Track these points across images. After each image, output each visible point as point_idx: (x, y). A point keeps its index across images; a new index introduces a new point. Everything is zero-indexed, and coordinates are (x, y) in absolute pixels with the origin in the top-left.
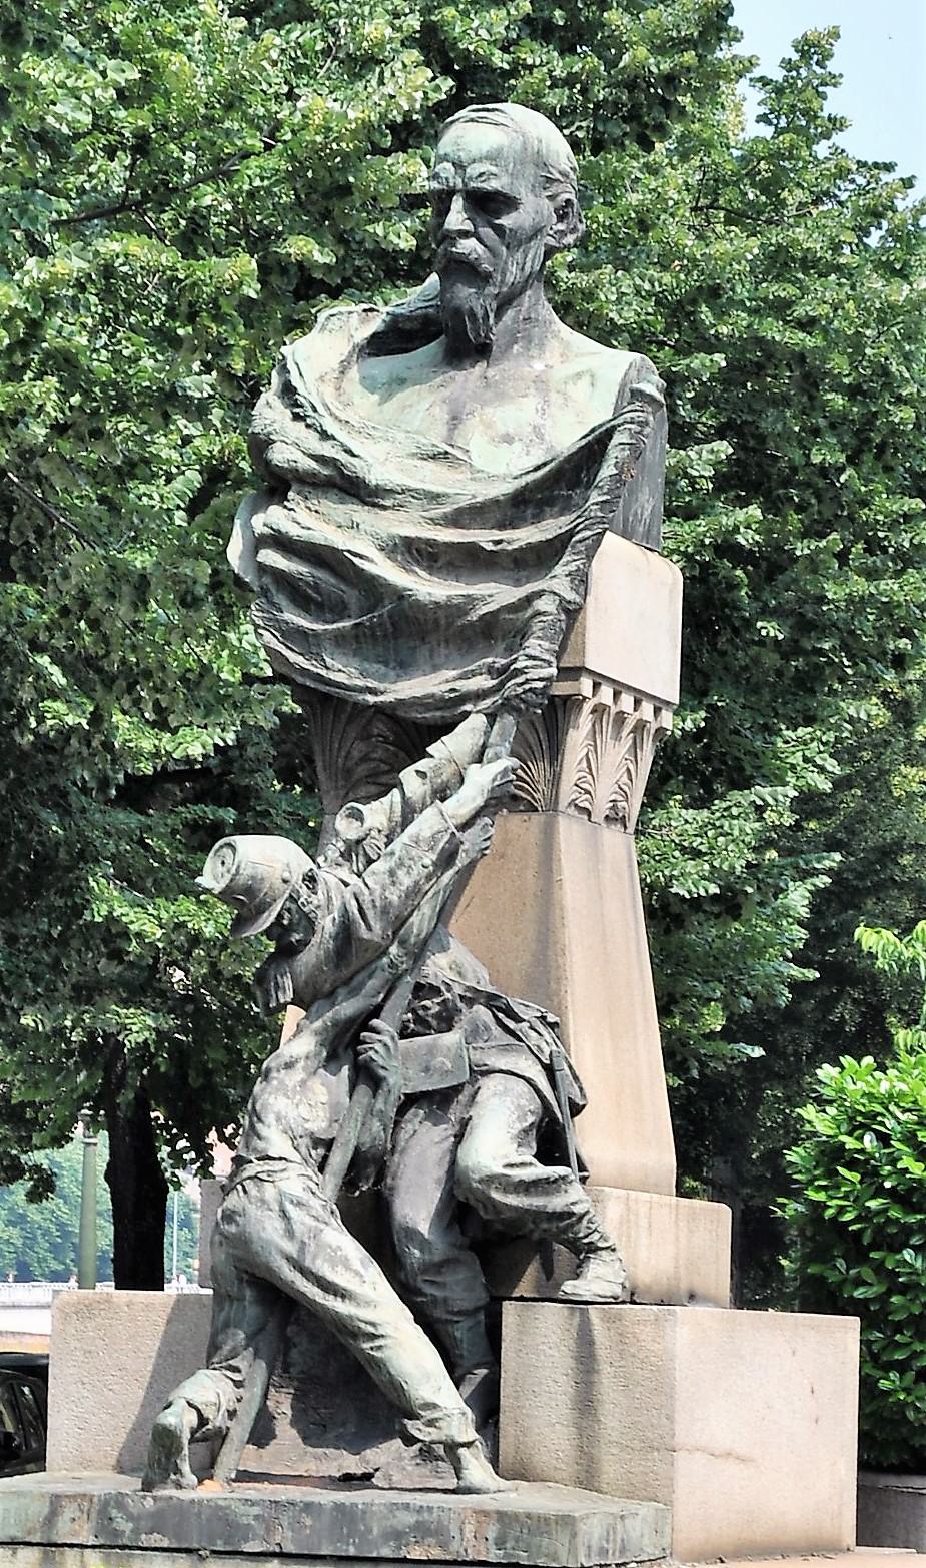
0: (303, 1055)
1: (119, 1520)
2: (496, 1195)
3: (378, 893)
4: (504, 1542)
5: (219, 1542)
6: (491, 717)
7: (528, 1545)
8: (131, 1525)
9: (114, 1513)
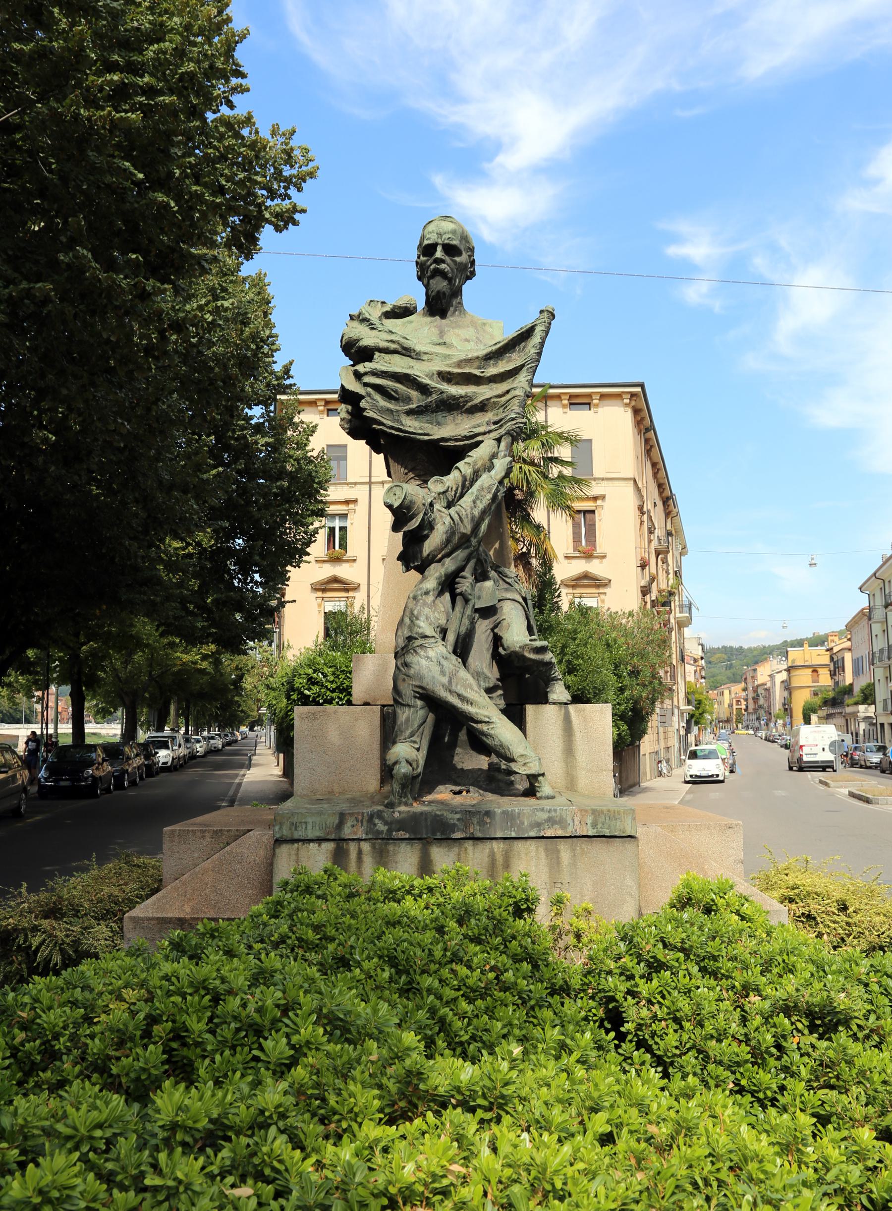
2: (527, 654)
6: (499, 440)
7: (609, 826)
8: (386, 827)
9: (377, 821)
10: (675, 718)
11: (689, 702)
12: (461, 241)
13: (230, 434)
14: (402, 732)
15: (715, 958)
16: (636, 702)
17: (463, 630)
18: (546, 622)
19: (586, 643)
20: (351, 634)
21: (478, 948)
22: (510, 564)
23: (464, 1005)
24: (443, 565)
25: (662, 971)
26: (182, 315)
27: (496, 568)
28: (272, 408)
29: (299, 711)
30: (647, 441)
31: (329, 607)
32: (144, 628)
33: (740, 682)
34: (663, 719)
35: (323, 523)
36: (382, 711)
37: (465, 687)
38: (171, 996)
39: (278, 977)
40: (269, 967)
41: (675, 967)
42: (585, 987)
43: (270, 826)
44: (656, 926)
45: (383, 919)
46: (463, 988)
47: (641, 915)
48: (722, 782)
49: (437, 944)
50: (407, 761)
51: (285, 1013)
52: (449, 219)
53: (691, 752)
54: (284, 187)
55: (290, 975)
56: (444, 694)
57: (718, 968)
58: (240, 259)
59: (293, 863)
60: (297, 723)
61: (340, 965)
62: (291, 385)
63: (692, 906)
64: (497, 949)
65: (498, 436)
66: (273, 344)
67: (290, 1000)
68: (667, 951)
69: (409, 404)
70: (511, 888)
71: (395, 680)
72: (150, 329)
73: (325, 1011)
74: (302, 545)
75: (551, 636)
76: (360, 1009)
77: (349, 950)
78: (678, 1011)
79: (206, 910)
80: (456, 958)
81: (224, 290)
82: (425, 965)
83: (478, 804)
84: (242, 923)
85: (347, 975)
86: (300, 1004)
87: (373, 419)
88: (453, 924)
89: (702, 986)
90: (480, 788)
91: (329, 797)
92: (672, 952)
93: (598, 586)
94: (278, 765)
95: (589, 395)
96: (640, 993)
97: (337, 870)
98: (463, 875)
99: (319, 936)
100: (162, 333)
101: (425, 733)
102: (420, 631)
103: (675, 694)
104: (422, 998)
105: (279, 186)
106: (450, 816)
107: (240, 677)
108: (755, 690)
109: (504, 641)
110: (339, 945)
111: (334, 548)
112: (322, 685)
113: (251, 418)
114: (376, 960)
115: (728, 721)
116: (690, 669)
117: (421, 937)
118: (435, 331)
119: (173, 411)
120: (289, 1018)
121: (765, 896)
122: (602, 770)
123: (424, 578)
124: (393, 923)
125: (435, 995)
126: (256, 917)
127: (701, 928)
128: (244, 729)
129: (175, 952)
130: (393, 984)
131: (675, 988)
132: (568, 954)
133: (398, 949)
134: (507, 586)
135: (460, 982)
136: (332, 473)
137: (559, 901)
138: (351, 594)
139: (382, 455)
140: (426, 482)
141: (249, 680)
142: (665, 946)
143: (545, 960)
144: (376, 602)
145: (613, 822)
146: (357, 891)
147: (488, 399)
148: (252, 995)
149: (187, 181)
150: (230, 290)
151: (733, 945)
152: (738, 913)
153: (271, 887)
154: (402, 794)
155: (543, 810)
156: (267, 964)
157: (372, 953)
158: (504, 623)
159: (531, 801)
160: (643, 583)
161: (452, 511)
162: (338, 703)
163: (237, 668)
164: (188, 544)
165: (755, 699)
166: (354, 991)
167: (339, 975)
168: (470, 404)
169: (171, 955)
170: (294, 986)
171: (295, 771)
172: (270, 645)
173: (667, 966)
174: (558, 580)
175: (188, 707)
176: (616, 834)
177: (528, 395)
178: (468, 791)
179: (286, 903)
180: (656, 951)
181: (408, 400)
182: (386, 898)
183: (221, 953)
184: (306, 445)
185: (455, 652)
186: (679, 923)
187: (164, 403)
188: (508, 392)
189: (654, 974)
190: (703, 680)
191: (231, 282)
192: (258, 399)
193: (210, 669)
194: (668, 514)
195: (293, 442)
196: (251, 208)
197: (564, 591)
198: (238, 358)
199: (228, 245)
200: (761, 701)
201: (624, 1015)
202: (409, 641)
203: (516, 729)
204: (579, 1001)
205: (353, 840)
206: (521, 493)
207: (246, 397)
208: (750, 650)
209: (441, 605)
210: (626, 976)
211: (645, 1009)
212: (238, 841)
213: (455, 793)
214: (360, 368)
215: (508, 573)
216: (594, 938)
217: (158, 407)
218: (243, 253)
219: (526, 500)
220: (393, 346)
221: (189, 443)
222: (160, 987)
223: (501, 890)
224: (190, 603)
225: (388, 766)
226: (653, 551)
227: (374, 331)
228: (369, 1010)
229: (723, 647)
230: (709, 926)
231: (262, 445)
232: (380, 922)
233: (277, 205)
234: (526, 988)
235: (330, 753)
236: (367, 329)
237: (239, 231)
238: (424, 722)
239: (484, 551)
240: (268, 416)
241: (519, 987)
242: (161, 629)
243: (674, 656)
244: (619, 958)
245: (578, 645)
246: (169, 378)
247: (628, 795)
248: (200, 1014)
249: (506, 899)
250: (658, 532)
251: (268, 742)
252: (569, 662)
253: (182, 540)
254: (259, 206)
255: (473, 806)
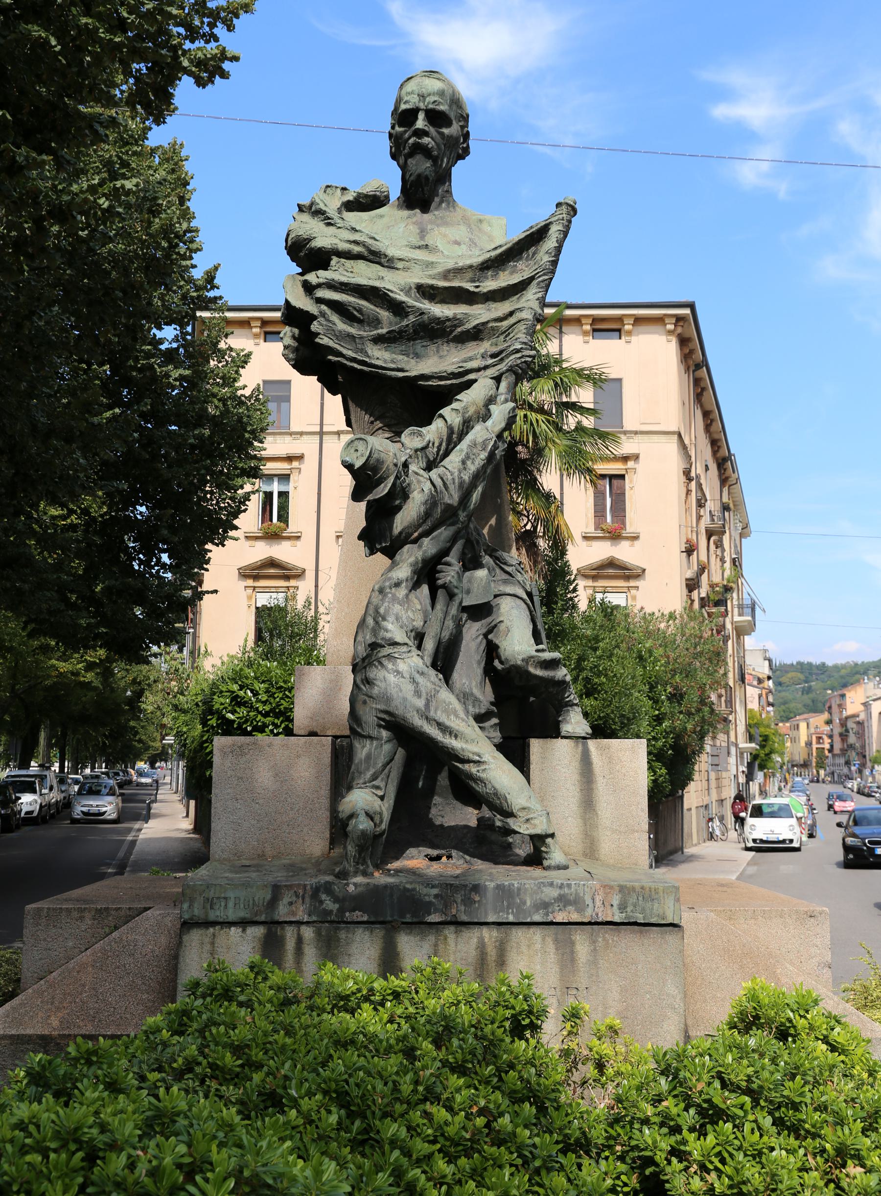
0: (404, 578)
1: (328, 902)
2: (532, 670)
3: (456, 474)
4: (625, 907)
5: (408, 916)
6: (498, 379)
8: (337, 906)
9: (324, 897)
10: (732, 760)
11: (751, 738)
12: (450, 106)
13: (131, 363)
14: (360, 773)
15: (796, 1107)
16: (678, 737)
17: (446, 635)
18: (557, 624)
19: (611, 655)
20: (291, 637)
21: (461, 1081)
22: (510, 548)
23: (442, 1165)
24: (420, 547)
25: (721, 1122)
26: (66, 198)
27: (491, 553)
28: (189, 329)
29: (220, 742)
30: (697, 381)
31: (263, 600)
32: (6, 625)
33: (822, 712)
34: (716, 759)
35: (257, 487)
36: (333, 743)
37: (448, 712)
38: (27, 1153)
39: (182, 1122)
40: (170, 1106)
41: (739, 1117)
42: (612, 1142)
43: (176, 901)
44: (710, 1056)
45: (331, 1037)
46: (441, 1139)
47: (687, 1038)
48: (798, 850)
49: (405, 1074)
50: (367, 814)
51: (190, 1177)
52: (436, 75)
53: (754, 806)
54: (209, 24)
55: (199, 1119)
56: (418, 722)
57: (800, 1120)
58: (147, 123)
59: (206, 955)
60: (216, 759)
61: (269, 1103)
62: (216, 298)
63: (760, 1027)
64: (487, 1083)
65: (497, 374)
66: (192, 241)
67: (198, 1157)
68: (727, 1093)
69: (377, 329)
70: (508, 994)
71: (353, 701)
72: (21, 216)
73: (246, 1173)
74: (227, 515)
75: (564, 645)
76: (296, 1171)
77: (281, 1082)
78: (744, 1183)
79: (81, 1024)
80: (431, 1096)
81: (125, 164)
82: (387, 1105)
83: (463, 874)
84: (132, 1042)
85: (278, 1120)
86: (211, 1164)
87: (329, 347)
88: (427, 1045)
89: (777, 1147)
90: (466, 852)
91: (259, 862)
92: (733, 1095)
93: (628, 578)
94: (187, 816)
95: (620, 319)
96: (690, 1153)
97: (268, 965)
98: (441, 974)
99: (240, 1062)
100: (38, 222)
101: (392, 775)
102: (388, 635)
103: (732, 727)
104: (383, 1154)
105: (202, 23)
106: (425, 891)
107: (139, 694)
108: (843, 723)
109: (501, 651)
110: (268, 1074)
111: (271, 520)
112: (252, 707)
113: (161, 341)
114: (319, 1097)
115: (805, 765)
116: (752, 692)
117: (382, 1063)
118: (414, 229)
119: (52, 330)
120: (196, 1185)
121: (864, 1017)
122: (634, 831)
123: (394, 565)
124: (344, 1043)
125: (402, 1149)
126: (153, 1033)
127: (774, 1061)
128: (141, 765)
129: (33, 1088)
130: (343, 1133)
131: (740, 1148)
132: (586, 1092)
133: (351, 1081)
134: (506, 577)
135: (436, 1131)
136: (270, 419)
137: (574, 1015)
138: (293, 583)
139: (339, 397)
140: (399, 434)
141: (151, 698)
142: (724, 1085)
143: (555, 1100)
144: (327, 595)
145: (649, 904)
146: (295, 996)
147: (484, 324)
148: (144, 1150)
149: (74, 10)
150: (134, 165)
151: (821, 1088)
152: (825, 1040)
153: (175, 989)
154: (360, 860)
155: (551, 884)
156: (166, 1103)
157: (314, 1087)
158: (502, 627)
159: (536, 872)
160: (689, 574)
161: (434, 474)
162: (272, 731)
163: (134, 681)
164: (71, 512)
165: (844, 736)
166: (288, 1144)
167: (267, 1119)
168: (459, 330)
169: (28, 1091)
170: (204, 1136)
171: (213, 825)
172: (181, 650)
173: (728, 1115)
174: (574, 568)
175: (64, 735)
176: (653, 920)
177: (540, 319)
178: (449, 857)
179: (195, 1012)
180: (711, 1092)
181: (376, 322)
182: (335, 1006)
183: (101, 1087)
184: (235, 380)
185: (434, 665)
186: (743, 1052)
187: (40, 318)
188: (511, 314)
189: (709, 1127)
190: (770, 709)
191: (135, 153)
192: (171, 315)
193: (97, 683)
194: (724, 480)
195: (217, 375)
196: (164, 52)
197: (581, 583)
198: (144, 259)
199: (131, 102)
200: (852, 739)
201: (667, 1186)
202: (372, 650)
203: (516, 771)
204: (603, 1163)
205: (291, 923)
206: (526, 451)
207: (155, 313)
208: (836, 668)
209: (416, 601)
210: (670, 1127)
211: (697, 1179)
212: (130, 924)
213: (432, 859)
214: (312, 278)
215: (508, 559)
216: (623, 1069)
217: (33, 322)
218: (151, 114)
219: (532, 459)
220: (357, 249)
221: (75, 371)
222: (12, 1141)
223: (494, 997)
224: (72, 592)
225: (341, 820)
226: (703, 531)
227: (331, 228)
228: (308, 1173)
229: (799, 663)
230: (786, 1058)
231: (176, 379)
232: (326, 1041)
233: (199, 49)
234: (529, 1141)
235: (261, 801)
236: (321, 225)
237: (147, 84)
238: (391, 760)
239: (475, 528)
240: (184, 339)
241: (519, 1140)
242: (30, 628)
243: (731, 675)
244: (657, 1100)
245: (600, 658)
246: (48, 285)
247: (667, 865)
248: (67, 1180)
249: (500, 1010)
250: (710, 505)
251: (174, 784)
252: (587, 680)
253: (63, 505)
254: (175, 49)
255: (457, 877)
